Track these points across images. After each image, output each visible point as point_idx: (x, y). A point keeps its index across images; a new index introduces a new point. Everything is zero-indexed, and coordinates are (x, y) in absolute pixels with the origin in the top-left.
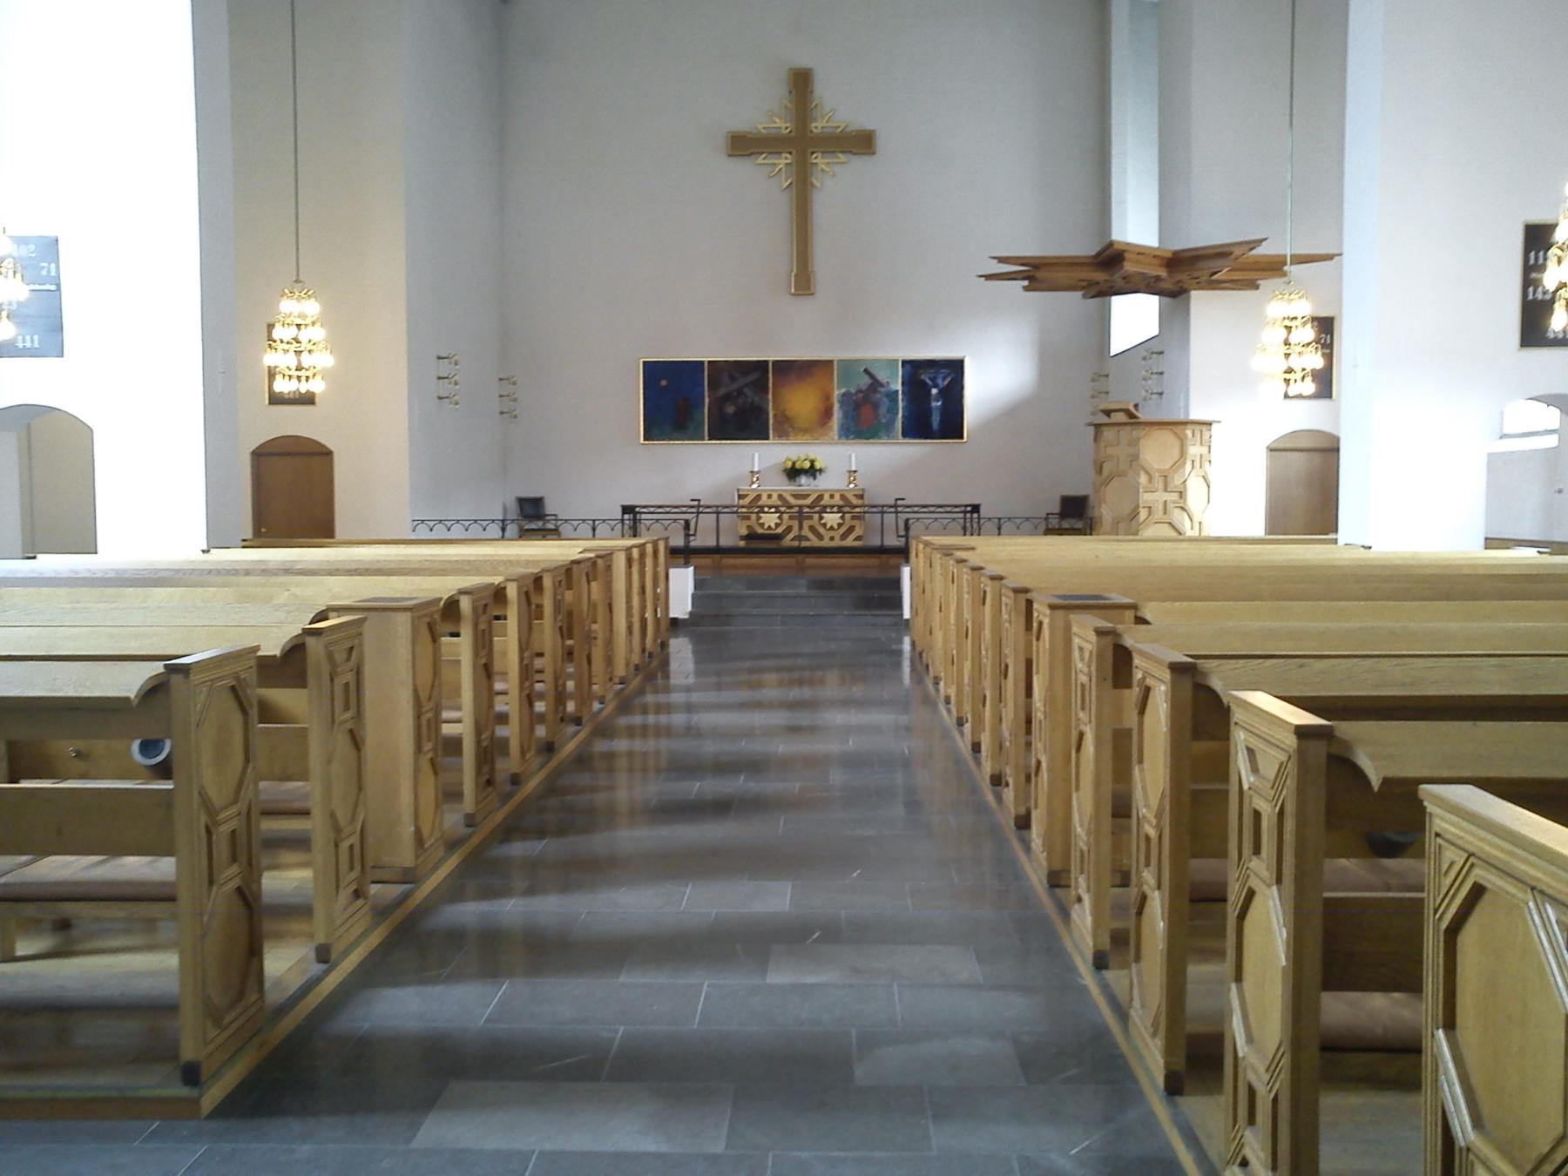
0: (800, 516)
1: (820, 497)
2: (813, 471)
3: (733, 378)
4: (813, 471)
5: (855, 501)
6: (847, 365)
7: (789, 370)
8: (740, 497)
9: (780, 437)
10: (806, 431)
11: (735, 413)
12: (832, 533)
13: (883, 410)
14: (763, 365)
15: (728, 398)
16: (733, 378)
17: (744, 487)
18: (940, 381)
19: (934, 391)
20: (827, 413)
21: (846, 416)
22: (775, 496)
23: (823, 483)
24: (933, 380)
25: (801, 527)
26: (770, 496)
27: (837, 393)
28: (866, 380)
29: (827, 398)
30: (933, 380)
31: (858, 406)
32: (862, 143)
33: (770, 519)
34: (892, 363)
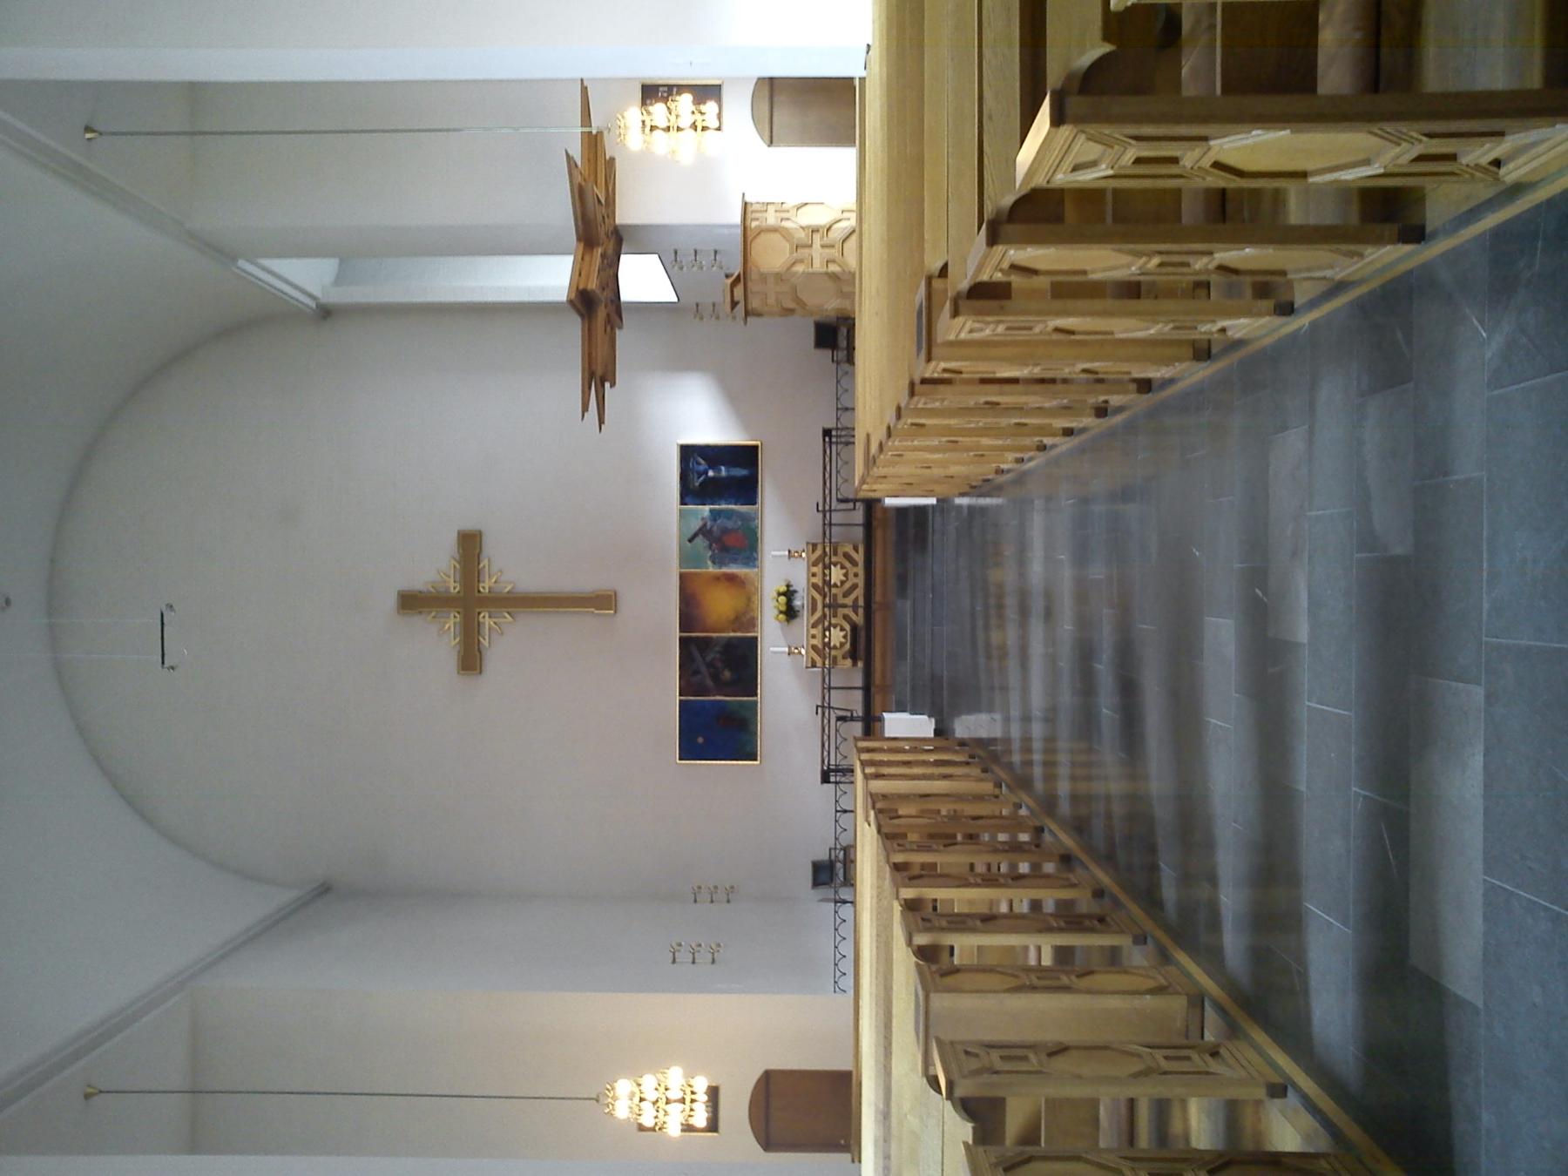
0: (833, 606)
1: (815, 586)
2: (789, 594)
3: (697, 672)
4: (789, 594)
5: (819, 552)
6: (684, 559)
7: (688, 619)
8: (814, 666)
10: (749, 599)
12: (851, 575)
13: (729, 524)
14: (684, 642)
15: (716, 677)
16: (697, 672)
18: (701, 468)
19: (711, 473)
20: (731, 579)
21: (734, 561)
22: (814, 631)
23: (801, 583)
25: (844, 606)
26: (814, 637)
27: (712, 569)
29: (717, 578)
32: (470, 544)
34: (682, 514)
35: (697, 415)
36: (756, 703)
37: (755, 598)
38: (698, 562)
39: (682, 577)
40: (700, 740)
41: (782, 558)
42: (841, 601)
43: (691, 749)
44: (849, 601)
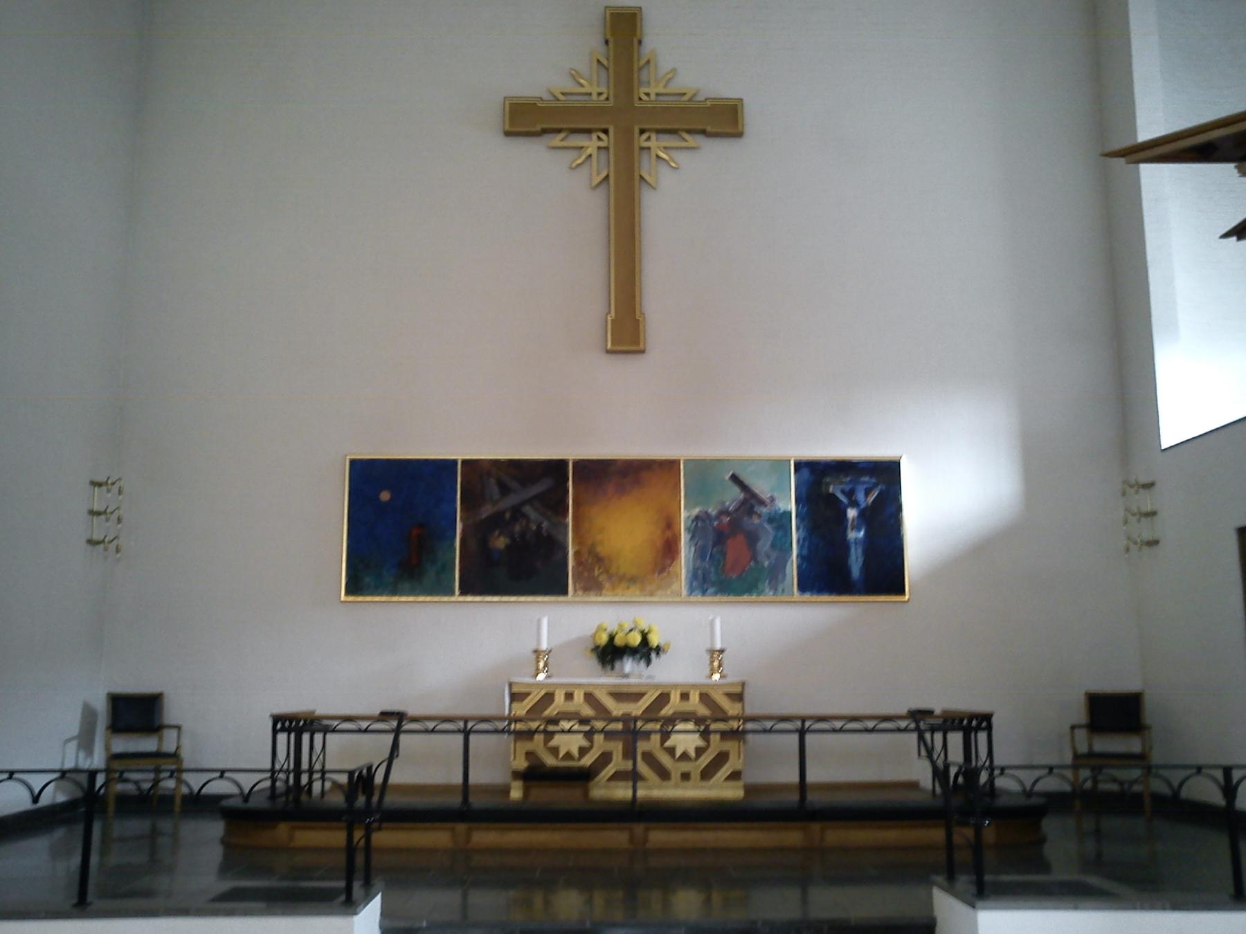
0: (630, 734)
1: (663, 698)
2: (645, 651)
3: (505, 490)
4: (645, 651)
6: (703, 469)
7: (601, 476)
8: (515, 697)
9: (586, 589)
10: (633, 580)
11: (508, 547)
12: (685, 767)
13: (764, 545)
14: (562, 464)
15: (496, 522)
16: (505, 490)
18: (860, 496)
19: (852, 513)
20: (669, 549)
21: (701, 554)
22: (579, 697)
29: (670, 524)
30: (850, 494)
31: (721, 538)
34: (778, 465)
35: (951, 493)
37: (634, 589)
38: (700, 489)
39: (670, 466)
41: (703, 638)
43: (368, 478)
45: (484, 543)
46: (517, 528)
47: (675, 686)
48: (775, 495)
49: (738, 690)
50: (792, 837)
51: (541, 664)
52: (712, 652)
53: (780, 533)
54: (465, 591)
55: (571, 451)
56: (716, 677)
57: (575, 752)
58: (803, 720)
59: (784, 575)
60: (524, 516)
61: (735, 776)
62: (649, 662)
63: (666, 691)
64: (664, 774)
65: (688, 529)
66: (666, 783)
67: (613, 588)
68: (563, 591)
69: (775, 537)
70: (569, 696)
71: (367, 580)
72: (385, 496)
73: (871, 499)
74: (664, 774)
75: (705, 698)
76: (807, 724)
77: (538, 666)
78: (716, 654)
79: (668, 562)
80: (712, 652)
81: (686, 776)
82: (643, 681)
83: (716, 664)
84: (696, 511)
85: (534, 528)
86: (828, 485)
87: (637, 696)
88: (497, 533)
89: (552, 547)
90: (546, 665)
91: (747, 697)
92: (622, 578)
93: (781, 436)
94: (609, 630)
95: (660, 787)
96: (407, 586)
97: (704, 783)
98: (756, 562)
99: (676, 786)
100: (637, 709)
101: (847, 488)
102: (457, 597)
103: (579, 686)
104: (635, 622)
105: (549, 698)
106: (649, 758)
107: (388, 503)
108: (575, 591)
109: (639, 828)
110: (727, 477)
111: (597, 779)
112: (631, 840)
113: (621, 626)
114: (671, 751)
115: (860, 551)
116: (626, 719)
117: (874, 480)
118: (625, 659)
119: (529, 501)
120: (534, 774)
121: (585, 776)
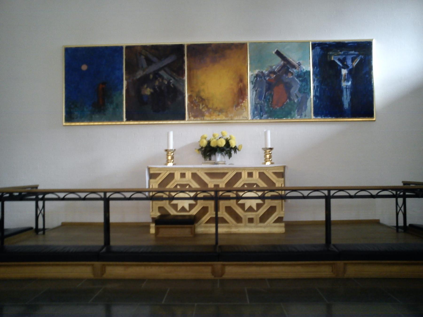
0: (217, 198)
1: (238, 176)
2: (228, 149)
3: (149, 62)
4: (228, 149)
6: (260, 47)
7: (204, 53)
8: (153, 176)
9: (195, 117)
10: (221, 111)
11: (152, 94)
12: (251, 215)
13: (295, 90)
14: (180, 47)
15: (145, 80)
16: (149, 62)
17: (157, 166)
18: (349, 62)
19: (344, 72)
20: (241, 93)
21: (259, 96)
22: (189, 175)
23: (237, 161)
24: (343, 61)
25: (217, 209)
28: (278, 62)
29: (241, 79)
30: (343, 61)
31: (270, 86)
33: (184, 205)
34: (303, 44)
36: (121, 119)
37: (222, 117)
38: (258, 60)
39: (241, 47)
40: (84, 67)
41: (260, 143)
42: (223, 204)
43: (75, 58)
44: (222, 213)
45: (138, 91)
46: (157, 83)
47: (244, 169)
48: (301, 62)
49: (282, 171)
50: (324, 270)
51: (170, 158)
52: (265, 149)
53: (304, 84)
54: (128, 119)
55: (186, 39)
56: (268, 163)
57: (187, 207)
58: (329, 190)
59: (306, 107)
60: (161, 76)
61: (279, 220)
62: (230, 156)
63: (172, 172)
64: (238, 219)
65: (252, 82)
66: (239, 224)
67: (211, 115)
68: (183, 118)
69: (301, 85)
70: (183, 175)
71: (76, 113)
72: (84, 67)
73: (355, 64)
74: (238, 219)
75: (262, 175)
76: (332, 192)
77: (167, 158)
78: (268, 150)
79: (241, 100)
80: (265, 149)
81: (251, 220)
82: (227, 166)
83: (268, 156)
84: (256, 72)
85: (166, 83)
86: (331, 56)
87: (222, 175)
88: (145, 86)
89: (176, 93)
90: (172, 158)
91: (287, 174)
92: (215, 110)
93: (303, 31)
94: (208, 139)
95: (236, 227)
96: (97, 116)
97: (262, 224)
98: (290, 100)
99: (246, 226)
100: (222, 183)
101: (341, 57)
102: (125, 122)
103: (188, 169)
104: (222, 133)
105: (171, 176)
106: (229, 210)
107: (87, 70)
108: (189, 117)
109: (218, 264)
110: (274, 53)
111: (200, 221)
112: (213, 272)
113: (214, 136)
114: (242, 206)
115: (348, 93)
116: (217, 190)
117: (357, 53)
118: (217, 154)
119: (162, 68)
120: (163, 220)
121: (191, 221)
